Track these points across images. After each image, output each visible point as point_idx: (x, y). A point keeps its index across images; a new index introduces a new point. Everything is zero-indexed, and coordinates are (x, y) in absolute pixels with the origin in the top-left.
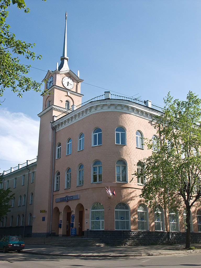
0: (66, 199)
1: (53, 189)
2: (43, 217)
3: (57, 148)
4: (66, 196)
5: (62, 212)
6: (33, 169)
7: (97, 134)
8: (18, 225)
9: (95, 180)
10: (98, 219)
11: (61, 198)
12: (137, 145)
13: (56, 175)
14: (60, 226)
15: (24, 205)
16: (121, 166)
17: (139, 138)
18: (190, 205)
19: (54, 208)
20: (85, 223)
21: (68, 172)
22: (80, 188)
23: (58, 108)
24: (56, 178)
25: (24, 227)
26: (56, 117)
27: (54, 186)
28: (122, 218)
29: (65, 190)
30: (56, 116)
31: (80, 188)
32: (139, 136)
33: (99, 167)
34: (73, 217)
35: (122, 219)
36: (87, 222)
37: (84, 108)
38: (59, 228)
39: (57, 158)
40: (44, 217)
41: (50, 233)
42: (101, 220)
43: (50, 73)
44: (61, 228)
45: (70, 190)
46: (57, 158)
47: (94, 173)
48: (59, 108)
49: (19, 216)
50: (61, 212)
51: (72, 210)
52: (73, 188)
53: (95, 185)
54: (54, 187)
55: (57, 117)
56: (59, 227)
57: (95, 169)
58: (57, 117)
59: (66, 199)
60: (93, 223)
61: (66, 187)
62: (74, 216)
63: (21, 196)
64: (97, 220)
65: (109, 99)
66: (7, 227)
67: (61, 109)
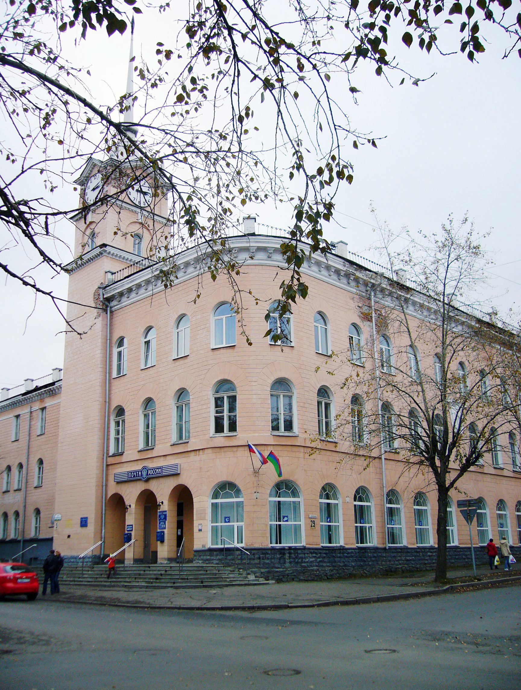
0: (144, 474)
1: (108, 450)
2: (82, 517)
3: (115, 351)
4: (144, 468)
5: (133, 506)
6: (42, 400)
7: (224, 317)
8: (15, 536)
9: (219, 428)
10: (229, 520)
11: (128, 472)
12: (317, 348)
13: (112, 418)
14: (128, 538)
15: (19, 490)
16: (282, 396)
17: (319, 328)
18: (447, 486)
19: (109, 495)
20: (196, 530)
21: (145, 409)
22: (180, 449)
23: (116, 252)
24: (113, 425)
25: (19, 541)
26: (113, 274)
27: (109, 443)
28: (286, 519)
29: (139, 452)
30: (114, 271)
31: (180, 449)
32: (319, 326)
33: (229, 397)
34: (163, 517)
35: (287, 521)
36: (200, 527)
37: (190, 255)
38: (159, 542)
39: (114, 375)
40: (85, 518)
41: (102, 556)
42: (236, 524)
43: (95, 165)
44: (162, 541)
45: (154, 453)
46: (114, 375)
47: (217, 412)
48: (120, 253)
49: (5, 515)
50: (130, 506)
51: (159, 500)
52: (161, 448)
53: (220, 440)
54: (108, 447)
55: (115, 273)
56: (157, 541)
57: (219, 402)
58: (115, 273)
59: (144, 474)
60: (215, 530)
61: (141, 446)
62: (165, 515)
63: (9, 468)
64: (226, 522)
65: (253, 234)
66: (42, 536)
67: (123, 254)
